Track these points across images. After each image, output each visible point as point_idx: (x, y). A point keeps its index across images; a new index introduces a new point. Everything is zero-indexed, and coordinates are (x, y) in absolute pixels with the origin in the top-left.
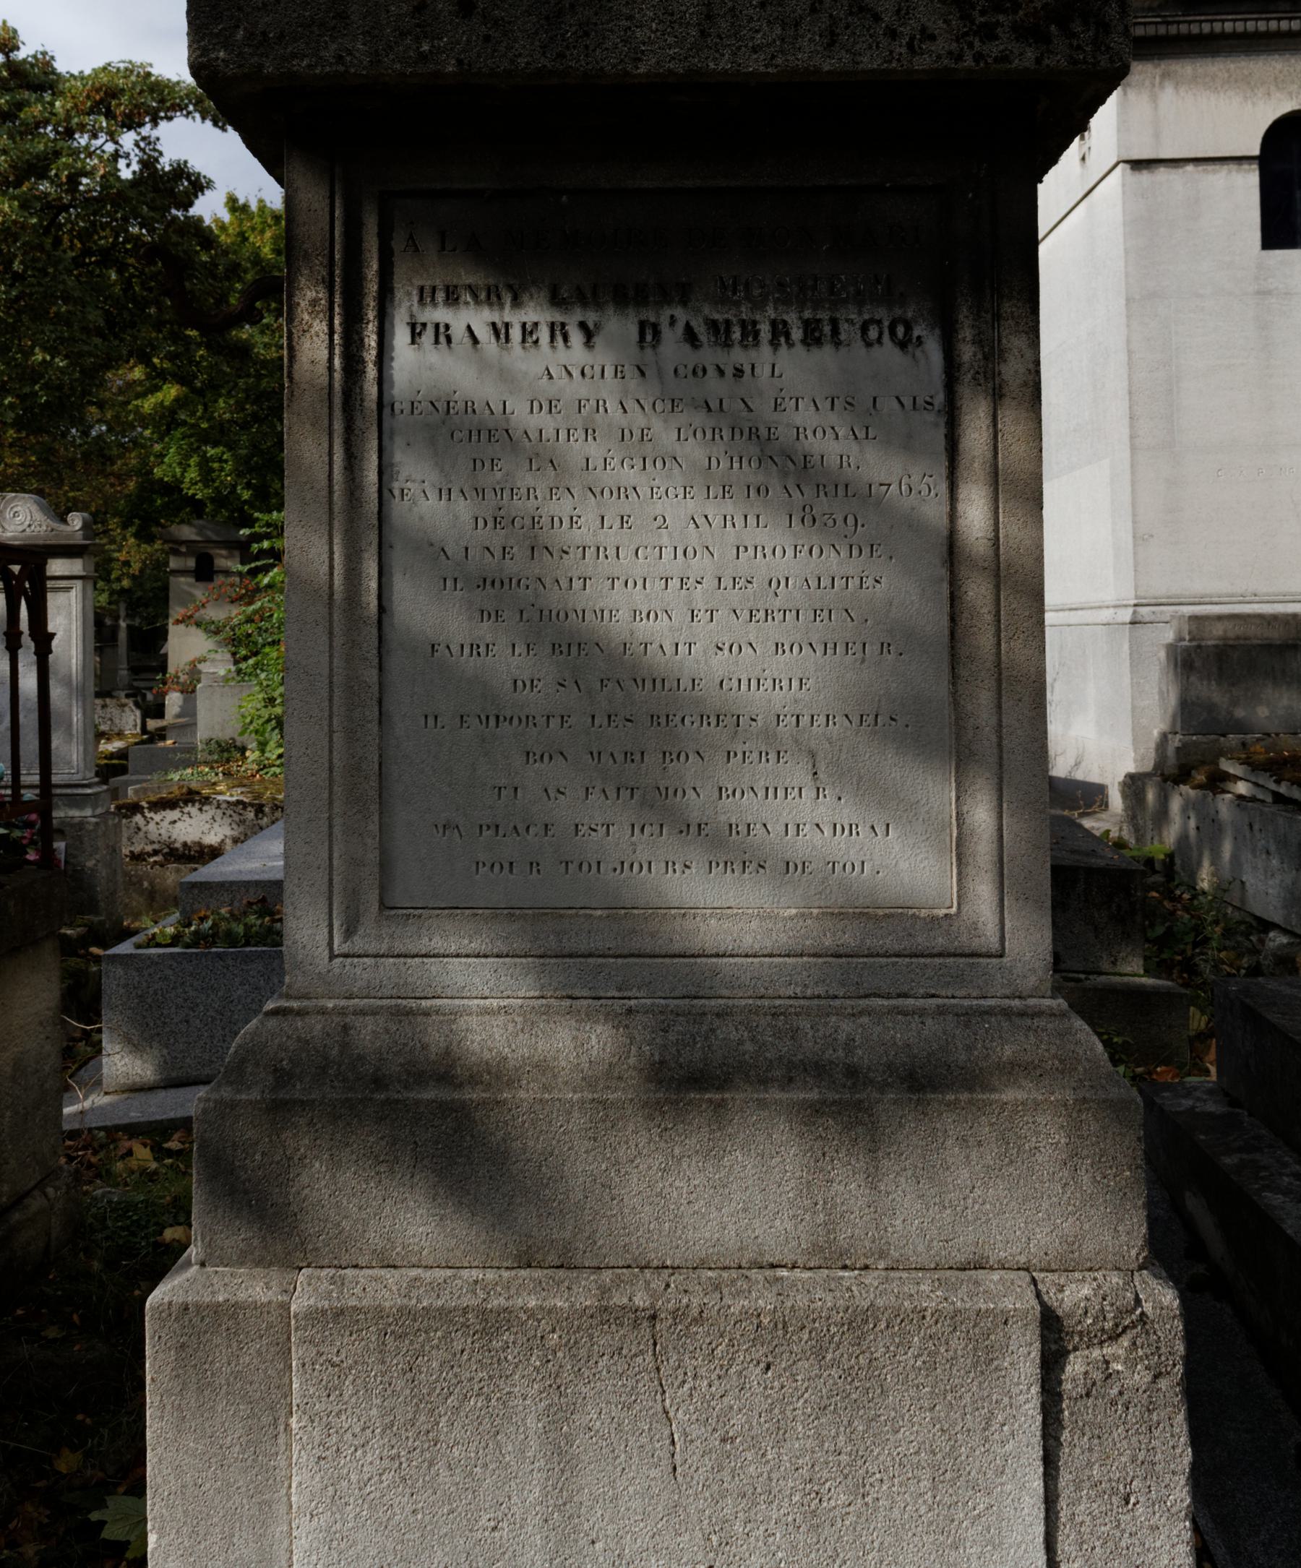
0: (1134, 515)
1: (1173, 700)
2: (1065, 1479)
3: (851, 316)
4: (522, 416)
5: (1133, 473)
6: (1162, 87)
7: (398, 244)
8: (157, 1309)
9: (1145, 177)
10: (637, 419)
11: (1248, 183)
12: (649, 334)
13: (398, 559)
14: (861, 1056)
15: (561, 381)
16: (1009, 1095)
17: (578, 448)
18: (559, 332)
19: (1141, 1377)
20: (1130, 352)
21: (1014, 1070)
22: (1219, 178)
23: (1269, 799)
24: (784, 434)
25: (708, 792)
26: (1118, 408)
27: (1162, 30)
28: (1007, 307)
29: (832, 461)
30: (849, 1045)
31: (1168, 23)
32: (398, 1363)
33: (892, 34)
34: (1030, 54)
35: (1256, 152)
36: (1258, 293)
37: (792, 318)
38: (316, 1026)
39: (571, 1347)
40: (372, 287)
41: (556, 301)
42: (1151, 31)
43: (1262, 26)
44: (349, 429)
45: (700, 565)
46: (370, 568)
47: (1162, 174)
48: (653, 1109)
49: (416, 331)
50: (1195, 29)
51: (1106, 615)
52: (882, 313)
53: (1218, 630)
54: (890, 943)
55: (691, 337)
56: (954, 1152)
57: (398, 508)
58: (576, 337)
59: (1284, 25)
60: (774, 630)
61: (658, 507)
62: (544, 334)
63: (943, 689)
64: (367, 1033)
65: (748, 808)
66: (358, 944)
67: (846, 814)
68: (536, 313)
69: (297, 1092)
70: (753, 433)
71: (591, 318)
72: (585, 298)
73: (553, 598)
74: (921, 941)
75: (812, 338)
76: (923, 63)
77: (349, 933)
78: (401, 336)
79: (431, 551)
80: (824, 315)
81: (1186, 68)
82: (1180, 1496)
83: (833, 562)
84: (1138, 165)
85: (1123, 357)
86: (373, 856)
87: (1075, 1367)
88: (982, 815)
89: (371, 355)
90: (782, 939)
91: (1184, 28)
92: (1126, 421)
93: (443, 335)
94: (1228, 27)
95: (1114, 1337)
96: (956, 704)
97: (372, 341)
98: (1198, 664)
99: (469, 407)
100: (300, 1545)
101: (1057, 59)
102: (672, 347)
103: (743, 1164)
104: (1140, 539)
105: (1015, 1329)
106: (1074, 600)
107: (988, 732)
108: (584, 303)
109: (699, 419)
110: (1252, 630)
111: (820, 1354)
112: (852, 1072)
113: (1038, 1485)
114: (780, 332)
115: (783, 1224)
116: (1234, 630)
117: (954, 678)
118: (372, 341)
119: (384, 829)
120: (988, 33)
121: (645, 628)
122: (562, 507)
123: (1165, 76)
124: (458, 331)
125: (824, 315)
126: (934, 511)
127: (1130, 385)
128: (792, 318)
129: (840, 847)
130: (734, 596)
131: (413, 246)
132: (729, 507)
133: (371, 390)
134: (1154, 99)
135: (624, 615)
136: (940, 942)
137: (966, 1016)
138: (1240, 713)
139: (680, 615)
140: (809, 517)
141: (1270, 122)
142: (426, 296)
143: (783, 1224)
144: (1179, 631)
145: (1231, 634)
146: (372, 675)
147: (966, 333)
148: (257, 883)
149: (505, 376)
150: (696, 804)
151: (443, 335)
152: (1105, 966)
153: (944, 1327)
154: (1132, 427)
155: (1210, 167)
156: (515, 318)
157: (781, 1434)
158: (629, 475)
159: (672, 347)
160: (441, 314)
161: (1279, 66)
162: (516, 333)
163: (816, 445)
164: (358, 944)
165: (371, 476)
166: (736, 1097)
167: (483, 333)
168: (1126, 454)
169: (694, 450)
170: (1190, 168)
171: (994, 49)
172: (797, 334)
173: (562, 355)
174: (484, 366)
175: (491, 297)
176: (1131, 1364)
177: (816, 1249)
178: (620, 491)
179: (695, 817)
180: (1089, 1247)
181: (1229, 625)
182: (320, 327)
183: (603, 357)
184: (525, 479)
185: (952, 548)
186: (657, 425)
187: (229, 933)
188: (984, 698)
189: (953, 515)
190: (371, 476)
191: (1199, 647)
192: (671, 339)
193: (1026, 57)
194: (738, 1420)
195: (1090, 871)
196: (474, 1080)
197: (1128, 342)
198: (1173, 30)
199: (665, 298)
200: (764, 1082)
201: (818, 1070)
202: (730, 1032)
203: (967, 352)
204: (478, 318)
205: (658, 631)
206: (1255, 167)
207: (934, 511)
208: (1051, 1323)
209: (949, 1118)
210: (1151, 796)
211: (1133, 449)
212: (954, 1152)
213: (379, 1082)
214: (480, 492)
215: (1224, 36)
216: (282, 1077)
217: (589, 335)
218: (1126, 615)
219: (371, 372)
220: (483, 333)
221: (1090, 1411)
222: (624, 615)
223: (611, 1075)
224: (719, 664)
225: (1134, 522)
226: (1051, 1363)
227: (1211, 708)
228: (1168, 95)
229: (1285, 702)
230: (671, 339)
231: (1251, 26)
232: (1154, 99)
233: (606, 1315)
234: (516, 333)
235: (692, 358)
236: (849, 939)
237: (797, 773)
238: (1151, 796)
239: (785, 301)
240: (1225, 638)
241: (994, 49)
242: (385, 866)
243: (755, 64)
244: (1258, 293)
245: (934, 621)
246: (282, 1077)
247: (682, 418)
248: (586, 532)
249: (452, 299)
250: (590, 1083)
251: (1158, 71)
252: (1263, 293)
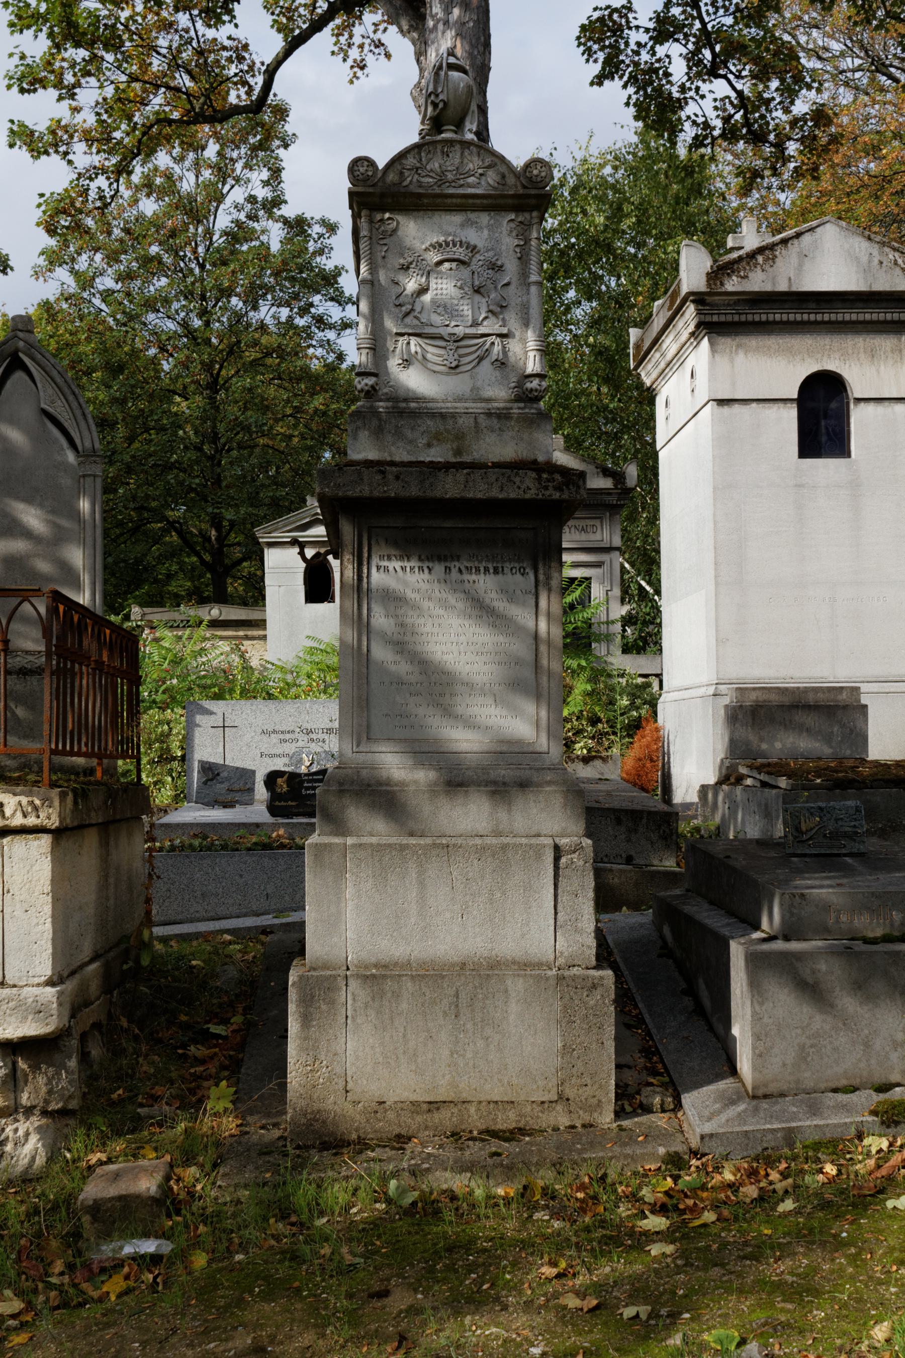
0: (717, 626)
1: (727, 739)
2: (560, 891)
3: (508, 566)
4: (410, 594)
5: (716, 599)
6: (737, 353)
7: (373, 542)
8: (310, 845)
9: (726, 410)
10: (444, 595)
11: (792, 413)
12: (448, 570)
13: (372, 636)
14: (507, 779)
15: (422, 584)
16: (548, 789)
17: (426, 604)
18: (421, 569)
19: (581, 863)
20: (715, 523)
21: (549, 783)
22: (772, 411)
23: (758, 785)
24: (487, 601)
25: (464, 705)
26: (709, 556)
27: (736, 318)
28: (553, 564)
29: (501, 609)
30: (504, 776)
31: (740, 314)
32: (377, 858)
33: (519, 488)
34: (558, 494)
35: (796, 396)
36: (796, 486)
37: (490, 566)
38: (350, 771)
39: (425, 854)
40: (366, 555)
41: (420, 560)
42: (729, 318)
43: (799, 317)
44: (359, 597)
45: (463, 638)
46: (365, 639)
47: (737, 408)
48: (447, 793)
49: (378, 568)
50: (757, 318)
51: (702, 691)
52: (516, 565)
53: (753, 696)
54: (517, 750)
55: (460, 571)
56: (532, 804)
57: (373, 621)
58: (426, 571)
59: (812, 317)
60: (483, 658)
61: (450, 621)
62: (416, 570)
63: (533, 676)
64: (364, 773)
65: (475, 710)
66: (361, 749)
67: (504, 713)
68: (414, 563)
69: (346, 787)
70: (478, 600)
71: (431, 565)
72: (430, 558)
73: (419, 648)
74: (525, 749)
75: (496, 571)
76: (527, 496)
77: (358, 746)
78: (374, 570)
79: (383, 635)
80: (500, 565)
81: (753, 341)
82: (591, 894)
83: (501, 639)
84: (722, 402)
85: (712, 525)
86: (365, 723)
87: (563, 860)
88: (544, 714)
89: (365, 575)
90: (485, 749)
91: (750, 318)
92: (713, 566)
93: (386, 569)
94: (778, 317)
95: (574, 852)
96: (537, 681)
97: (365, 571)
98: (740, 717)
99: (394, 591)
100: (349, 908)
101: (565, 496)
102: (454, 573)
103: (473, 807)
104: (720, 641)
105: (547, 849)
106: (687, 683)
107: (546, 688)
108: (428, 560)
109: (462, 596)
110: (773, 697)
111: (493, 856)
112: (504, 784)
113: (552, 891)
114: (486, 570)
115: (484, 824)
116: (762, 697)
117: (536, 673)
118: (365, 571)
119: (368, 716)
120: (546, 488)
121: (445, 657)
122: (421, 621)
123: (739, 346)
124: (391, 569)
125: (500, 565)
126: (531, 624)
127: (715, 543)
128: (490, 566)
129: (502, 722)
130: (472, 648)
131: (377, 542)
132: (471, 622)
133: (365, 585)
134: (732, 361)
135: (439, 653)
136: (531, 749)
137: (538, 770)
138: (764, 746)
139: (456, 654)
140: (494, 626)
141: (804, 377)
142: (381, 558)
143: (484, 824)
144: (731, 698)
145: (760, 699)
146: (365, 670)
147: (541, 571)
148: (198, 824)
149: (406, 583)
150: (460, 710)
151: (386, 569)
152: (656, 862)
153: (528, 848)
154: (716, 570)
155: (767, 405)
156: (408, 565)
157: (483, 877)
158: (441, 612)
159: (454, 573)
160: (385, 563)
161: (810, 342)
162: (408, 569)
163: (496, 604)
164: (361, 749)
165: (365, 611)
166: (471, 789)
167: (398, 569)
168: (713, 587)
169: (460, 605)
170: (754, 405)
171: (547, 493)
172: (491, 571)
173: (422, 576)
174: (398, 579)
175: (401, 558)
176: (579, 859)
177: (493, 831)
178: (439, 616)
179: (460, 713)
180: (569, 831)
181: (759, 693)
182: (350, 567)
183: (434, 577)
184: (410, 613)
185: (536, 636)
186: (450, 597)
187: (191, 845)
188: (545, 679)
189: (537, 625)
190: (365, 611)
191: (741, 706)
192: (454, 572)
193: (557, 495)
194: (471, 874)
195: (650, 813)
196: (396, 785)
197: (714, 515)
198: (743, 318)
199: (453, 560)
200: (479, 786)
201: (495, 783)
202: (470, 773)
203: (541, 577)
204: (397, 564)
205: (449, 658)
206: (795, 405)
207: (531, 624)
208: (557, 848)
209: (531, 795)
210: (710, 796)
211: (717, 584)
212: (532, 804)
213: (369, 785)
214: (397, 616)
215: (775, 323)
216: (341, 784)
217: (430, 570)
218: (711, 691)
219: (365, 580)
220: (398, 569)
221: (567, 872)
222: (439, 653)
223: (436, 784)
224: (468, 668)
225: (717, 631)
226: (557, 859)
227: (747, 743)
228: (740, 358)
229: (791, 740)
230: (454, 572)
231: (792, 317)
232: (732, 361)
233: (435, 846)
234: (408, 569)
235: (460, 577)
236: (504, 748)
237: (490, 701)
238: (710, 796)
239: (488, 561)
240: (757, 701)
241: (547, 493)
242: (368, 727)
243: (480, 496)
244: (796, 486)
245: (529, 657)
246: (341, 784)
247: (457, 595)
248: (428, 629)
249: (389, 558)
250: (430, 786)
251: (735, 343)
252: (799, 486)
